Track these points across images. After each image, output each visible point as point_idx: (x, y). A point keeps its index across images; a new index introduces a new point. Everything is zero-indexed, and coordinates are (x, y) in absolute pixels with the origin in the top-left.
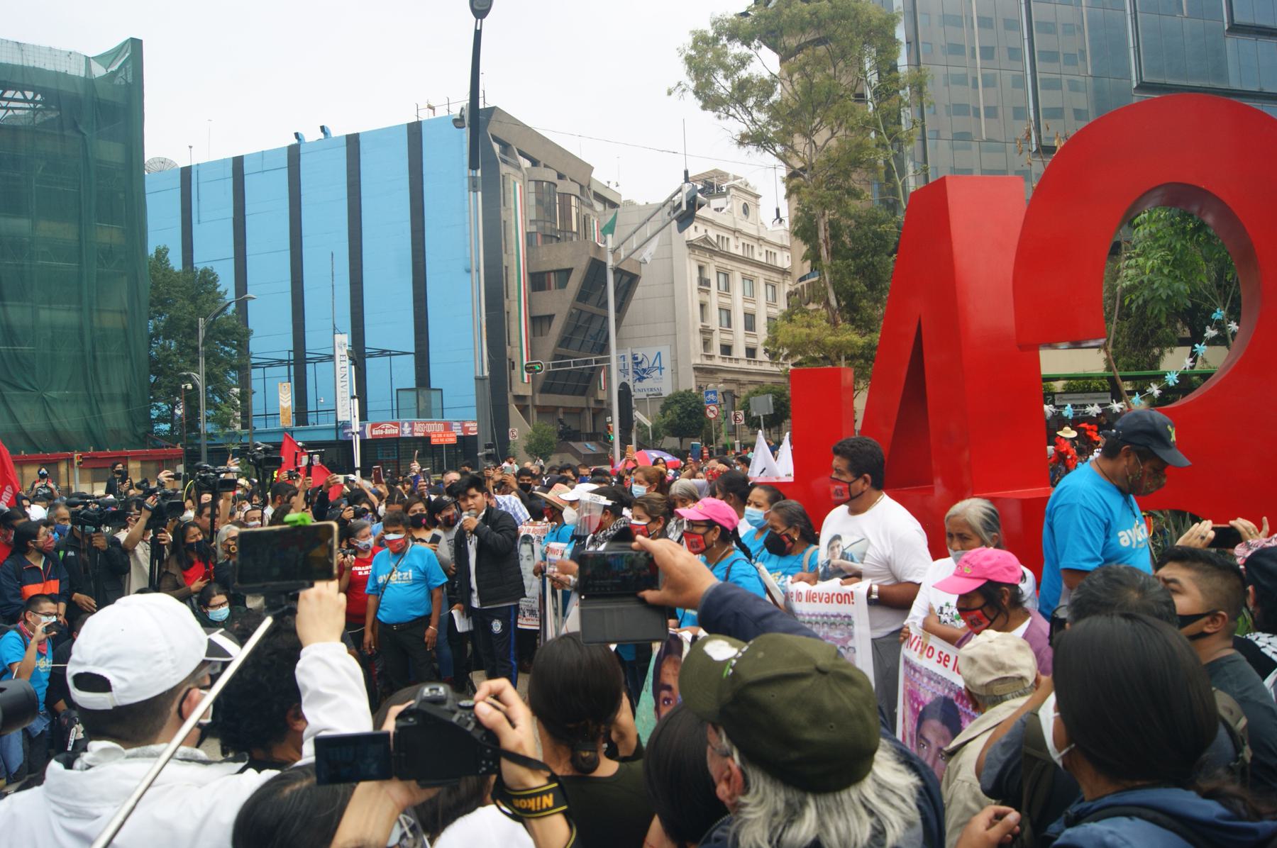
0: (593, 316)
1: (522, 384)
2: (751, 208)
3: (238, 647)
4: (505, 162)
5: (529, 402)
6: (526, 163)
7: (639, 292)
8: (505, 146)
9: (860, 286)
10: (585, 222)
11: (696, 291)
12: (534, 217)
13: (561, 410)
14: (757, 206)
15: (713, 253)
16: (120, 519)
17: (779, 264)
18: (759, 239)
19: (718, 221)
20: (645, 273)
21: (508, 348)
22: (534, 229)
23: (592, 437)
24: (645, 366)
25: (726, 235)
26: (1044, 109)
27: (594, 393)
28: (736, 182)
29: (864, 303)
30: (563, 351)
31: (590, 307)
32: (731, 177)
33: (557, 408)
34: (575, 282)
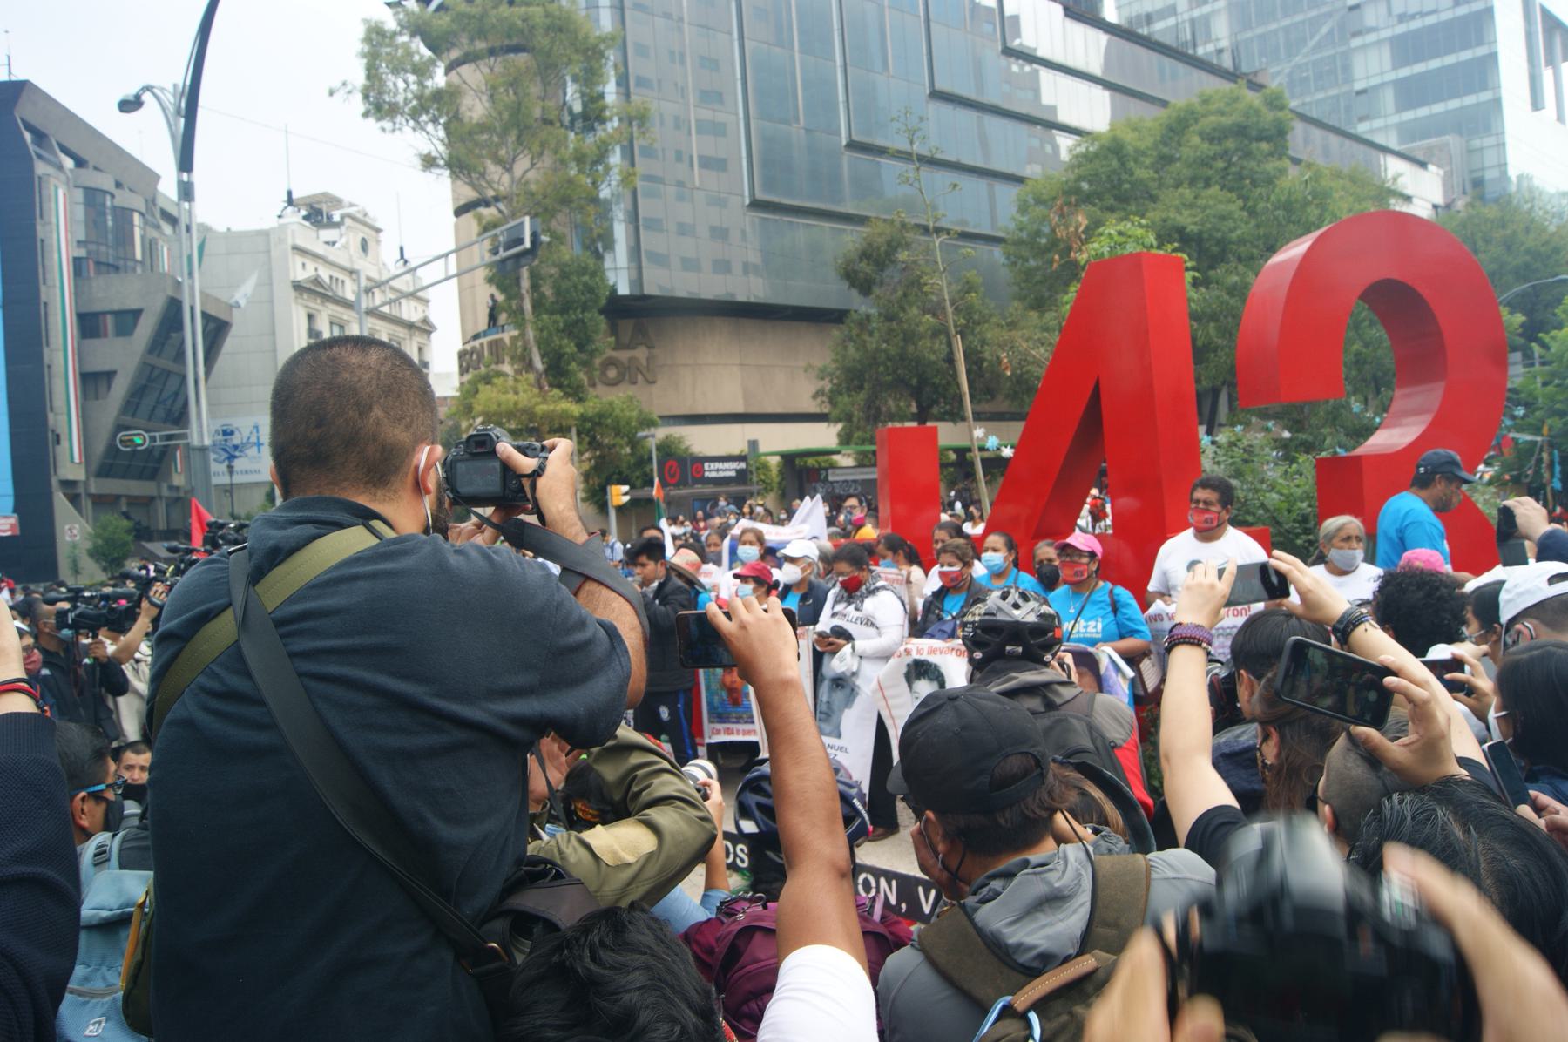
0: (168, 374)
1: (71, 461)
2: (371, 244)
3: (1048, 670)
4: (40, 157)
5: (81, 490)
6: (69, 163)
7: (229, 345)
8: (40, 137)
9: (570, 347)
10: (151, 247)
12: (82, 237)
13: (124, 501)
14: (378, 242)
16: (120, 622)
19: (331, 258)
20: (236, 319)
21: (51, 416)
22: (82, 253)
23: (169, 534)
24: (236, 440)
25: (341, 276)
27: (168, 476)
28: (352, 210)
29: (573, 366)
30: (127, 420)
31: (164, 363)
33: (118, 497)
34: (145, 329)
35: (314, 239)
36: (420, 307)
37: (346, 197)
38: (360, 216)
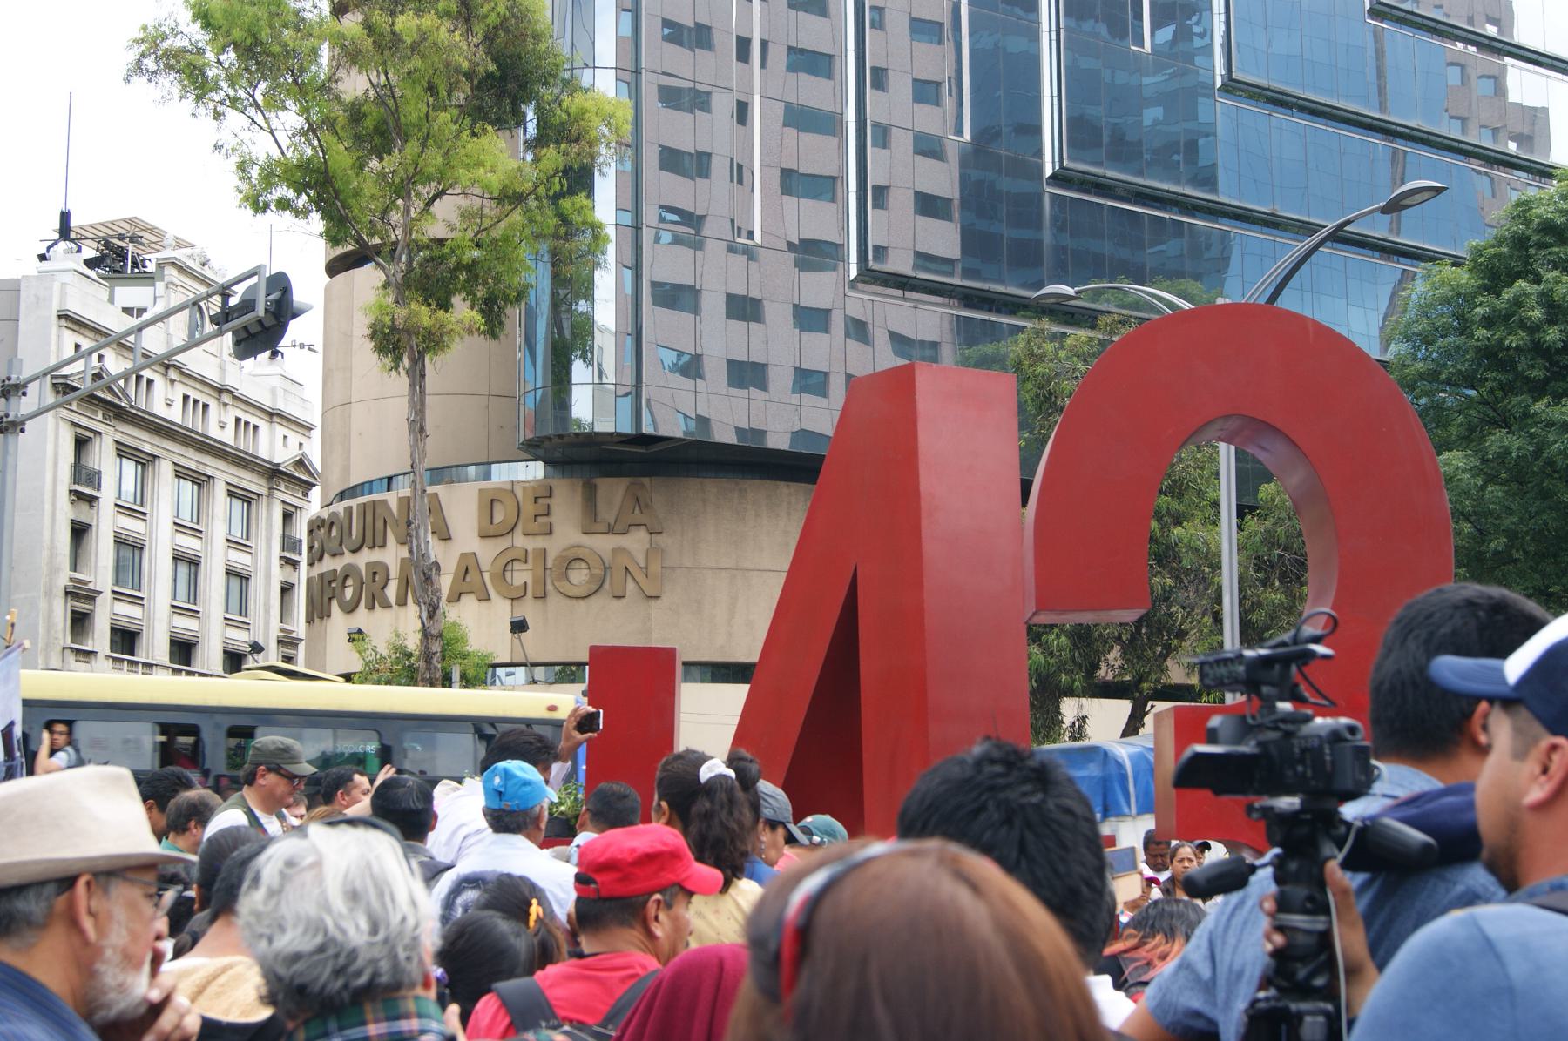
11: (276, 562)
15: (119, 413)
17: (263, 453)
18: (220, 391)
26: (1225, 236)
28: (181, 255)
32: (169, 240)
35: (104, 305)
36: (294, 438)
37: (172, 226)
38: (195, 265)
